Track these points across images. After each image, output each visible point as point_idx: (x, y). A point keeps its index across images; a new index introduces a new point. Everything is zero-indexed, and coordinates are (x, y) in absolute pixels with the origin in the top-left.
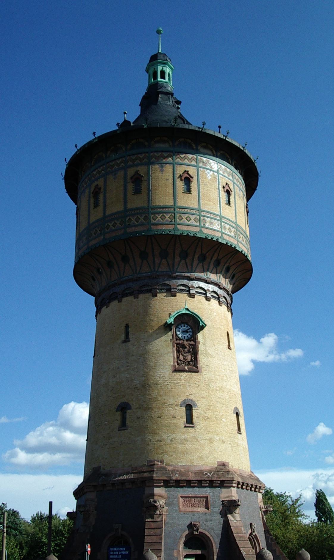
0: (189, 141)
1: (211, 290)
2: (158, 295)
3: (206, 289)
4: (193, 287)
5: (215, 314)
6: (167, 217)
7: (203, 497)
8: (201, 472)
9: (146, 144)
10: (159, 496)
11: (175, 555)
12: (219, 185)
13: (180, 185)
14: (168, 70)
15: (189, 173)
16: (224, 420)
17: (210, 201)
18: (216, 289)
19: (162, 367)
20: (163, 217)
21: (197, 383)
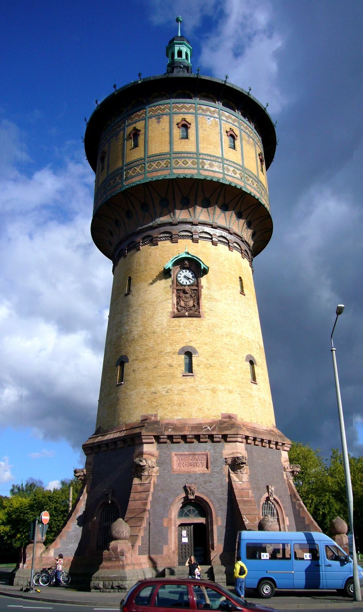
0: (188, 92)
1: (218, 235)
2: (159, 243)
3: (211, 233)
4: (196, 232)
5: (223, 258)
6: (163, 164)
7: (204, 455)
8: (199, 427)
9: (144, 101)
10: (149, 454)
11: (165, 524)
12: (221, 129)
13: (177, 132)
14: (184, 49)
15: (187, 120)
16: (232, 368)
17: (210, 145)
18: (225, 234)
19: (160, 315)
20: (158, 164)
21: (199, 329)
